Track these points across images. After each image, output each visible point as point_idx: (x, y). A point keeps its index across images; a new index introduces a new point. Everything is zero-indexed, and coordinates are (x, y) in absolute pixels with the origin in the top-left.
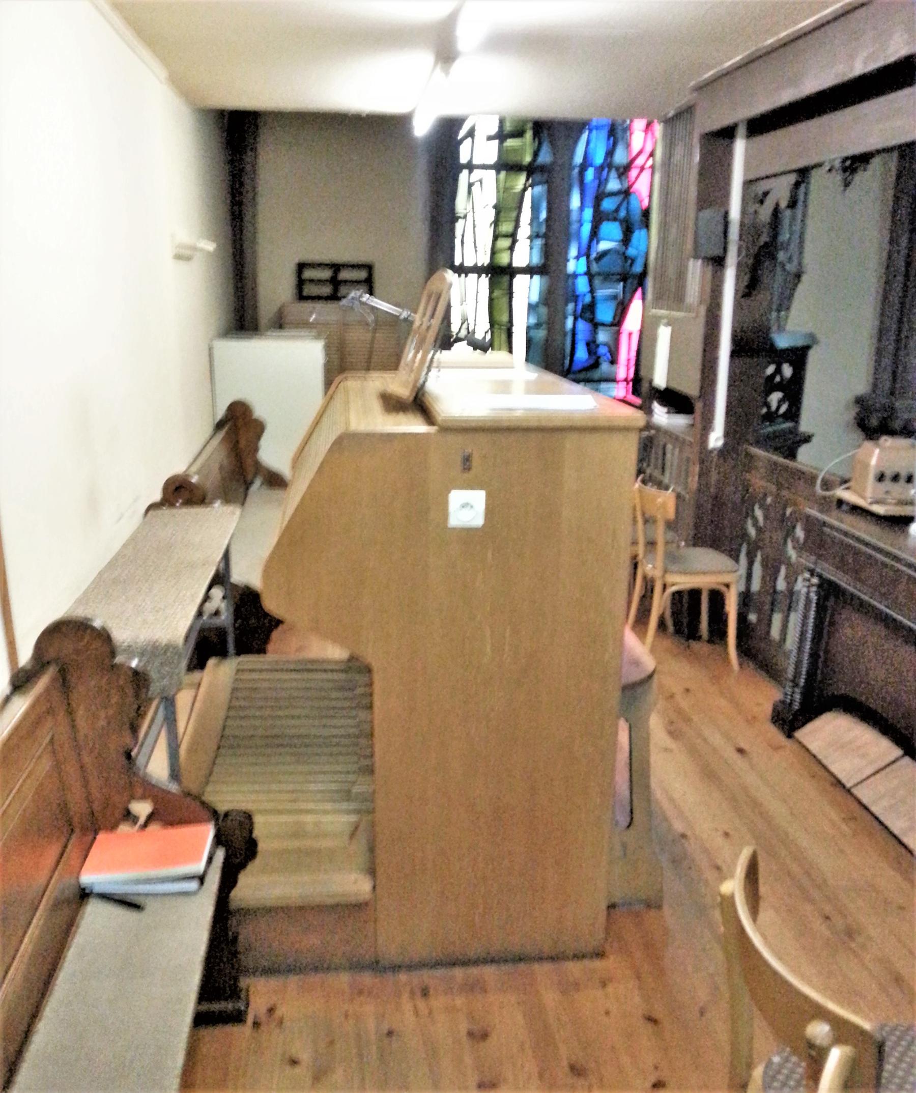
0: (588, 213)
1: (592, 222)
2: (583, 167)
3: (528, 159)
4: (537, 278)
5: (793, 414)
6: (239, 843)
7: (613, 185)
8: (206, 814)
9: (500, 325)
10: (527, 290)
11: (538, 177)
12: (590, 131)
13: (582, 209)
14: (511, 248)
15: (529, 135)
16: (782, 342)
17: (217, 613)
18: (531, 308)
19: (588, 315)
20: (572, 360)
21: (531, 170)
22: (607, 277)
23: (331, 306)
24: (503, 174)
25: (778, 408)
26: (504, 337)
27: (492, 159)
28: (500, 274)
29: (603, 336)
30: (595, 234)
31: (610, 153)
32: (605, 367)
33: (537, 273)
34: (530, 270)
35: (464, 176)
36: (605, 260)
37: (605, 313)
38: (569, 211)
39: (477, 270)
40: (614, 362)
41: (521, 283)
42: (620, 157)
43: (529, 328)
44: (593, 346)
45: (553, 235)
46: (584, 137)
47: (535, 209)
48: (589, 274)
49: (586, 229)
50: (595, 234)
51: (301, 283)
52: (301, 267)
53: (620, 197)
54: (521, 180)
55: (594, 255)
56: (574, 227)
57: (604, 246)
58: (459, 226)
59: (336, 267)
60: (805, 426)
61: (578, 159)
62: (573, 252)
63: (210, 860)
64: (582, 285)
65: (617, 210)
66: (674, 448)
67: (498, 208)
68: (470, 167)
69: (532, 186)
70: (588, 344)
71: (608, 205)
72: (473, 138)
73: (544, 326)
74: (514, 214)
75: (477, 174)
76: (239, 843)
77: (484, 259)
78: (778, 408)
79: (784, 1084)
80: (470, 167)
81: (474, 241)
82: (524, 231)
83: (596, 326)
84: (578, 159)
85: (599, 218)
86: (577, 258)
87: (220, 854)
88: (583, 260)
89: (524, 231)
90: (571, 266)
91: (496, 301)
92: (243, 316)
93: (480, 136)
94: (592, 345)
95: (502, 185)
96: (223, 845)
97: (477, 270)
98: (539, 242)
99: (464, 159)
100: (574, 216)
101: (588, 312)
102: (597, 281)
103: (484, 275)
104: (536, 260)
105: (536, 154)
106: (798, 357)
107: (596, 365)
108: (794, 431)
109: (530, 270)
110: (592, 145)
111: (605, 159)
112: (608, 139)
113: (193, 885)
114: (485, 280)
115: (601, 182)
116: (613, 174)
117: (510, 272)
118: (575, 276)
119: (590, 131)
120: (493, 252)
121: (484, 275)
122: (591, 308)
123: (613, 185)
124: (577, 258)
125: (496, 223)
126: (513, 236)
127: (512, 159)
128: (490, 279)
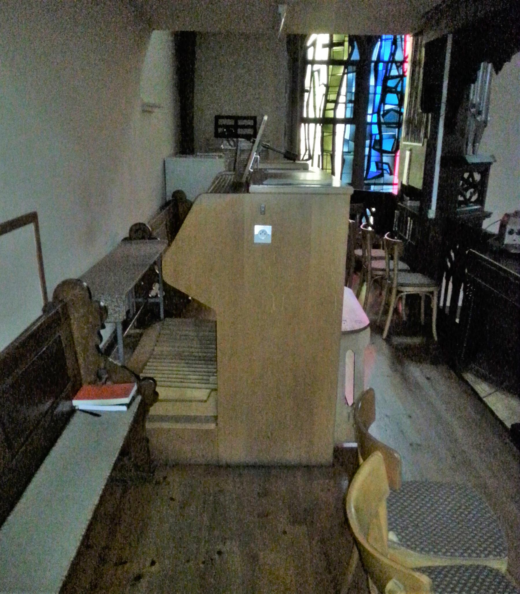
0: (379, 89)
1: (381, 95)
2: (377, 63)
3: (345, 58)
4: (348, 126)
5: (481, 201)
6: (148, 392)
7: (394, 72)
8: (133, 378)
9: (327, 151)
10: (343, 132)
11: (350, 68)
12: (381, 41)
13: (376, 86)
14: (335, 109)
15: (346, 44)
16: (472, 159)
17: (156, 296)
18: (345, 141)
19: (377, 147)
20: (367, 173)
21: (347, 64)
22: (389, 125)
23: (213, 134)
24: (331, 67)
25: (471, 197)
26: (329, 158)
27: (326, 58)
28: (328, 123)
29: (386, 159)
30: (383, 101)
31: (393, 54)
32: (387, 176)
33: (348, 123)
34: (346, 121)
35: (309, 67)
36: (387, 116)
37: (387, 145)
38: (368, 87)
39: (315, 121)
40: (391, 173)
41: (340, 128)
42: (399, 57)
43: (343, 153)
44: (380, 164)
45: (360, 100)
46: (379, 44)
47: (349, 86)
48: (379, 124)
49: (378, 98)
50: (383, 101)
51: (217, 126)
52: (218, 118)
53: (398, 79)
54: (341, 69)
55: (382, 113)
56: (371, 96)
57: (387, 107)
58: (306, 95)
59: (236, 118)
60: (487, 208)
61: (374, 58)
62: (370, 111)
63: (133, 399)
64: (375, 129)
65: (397, 86)
66: (411, 219)
67: (328, 87)
68: (313, 62)
69: (347, 73)
70: (377, 163)
71: (391, 83)
72: (315, 48)
73: (352, 153)
74: (337, 89)
75: (316, 67)
76: (148, 392)
77: (319, 115)
78: (471, 197)
79: (453, 590)
80: (313, 62)
81: (314, 104)
82: (342, 99)
83: (382, 152)
84: (374, 58)
85: (386, 90)
86: (372, 114)
87: (139, 398)
88: (375, 116)
89: (342, 99)
90: (369, 119)
91: (324, 138)
92: (186, 143)
93: (319, 45)
94: (379, 164)
95: (330, 73)
96: (141, 394)
97: (315, 121)
98: (350, 105)
99: (310, 57)
100: (372, 90)
101: (378, 145)
102: (383, 127)
103: (318, 125)
104: (349, 115)
105: (350, 55)
106: (484, 169)
107: (382, 175)
108: (481, 210)
109: (346, 121)
110: (382, 51)
111: (390, 58)
112: (392, 46)
113: (124, 408)
114: (319, 127)
115: (387, 70)
116: (394, 66)
117: (334, 121)
118: (371, 124)
119: (381, 41)
120: (325, 110)
121: (318, 125)
122: (380, 142)
123: (394, 72)
124: (372, 114)
125: (326, 95)
126: (336, 102)
127: (337, 58)
128: (322, 127)
